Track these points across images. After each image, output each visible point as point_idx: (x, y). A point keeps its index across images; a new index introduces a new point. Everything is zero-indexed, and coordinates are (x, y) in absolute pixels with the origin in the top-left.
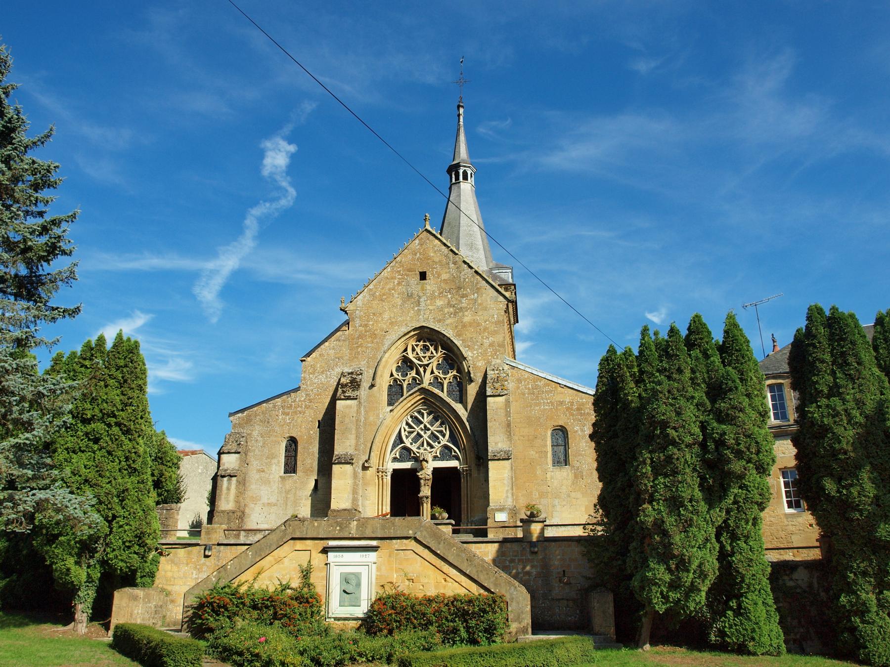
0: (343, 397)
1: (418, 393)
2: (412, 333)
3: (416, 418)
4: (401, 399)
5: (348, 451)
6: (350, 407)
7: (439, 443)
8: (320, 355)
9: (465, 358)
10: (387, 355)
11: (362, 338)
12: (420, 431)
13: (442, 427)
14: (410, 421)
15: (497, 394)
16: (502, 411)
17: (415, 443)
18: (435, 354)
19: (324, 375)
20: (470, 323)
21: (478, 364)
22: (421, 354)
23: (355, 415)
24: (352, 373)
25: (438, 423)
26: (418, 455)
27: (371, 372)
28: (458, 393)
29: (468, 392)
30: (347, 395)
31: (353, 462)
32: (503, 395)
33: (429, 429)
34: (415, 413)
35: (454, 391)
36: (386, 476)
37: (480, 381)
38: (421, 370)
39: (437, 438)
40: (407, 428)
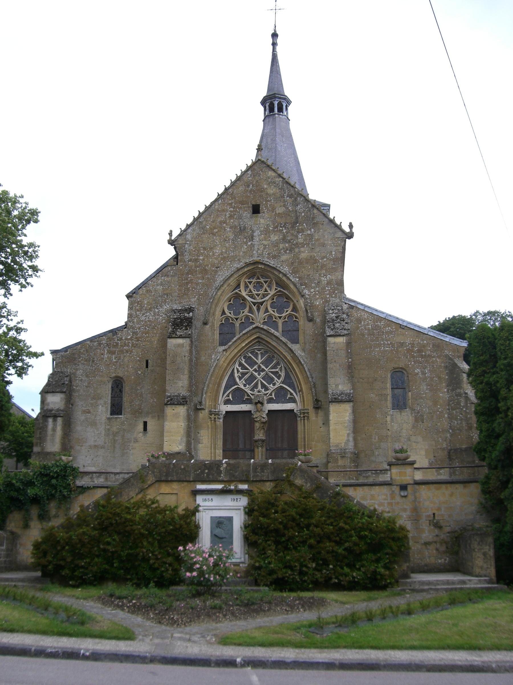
11: (192, 274)
20: (307, 259)
39: (273, 379)
40: (240, 368)
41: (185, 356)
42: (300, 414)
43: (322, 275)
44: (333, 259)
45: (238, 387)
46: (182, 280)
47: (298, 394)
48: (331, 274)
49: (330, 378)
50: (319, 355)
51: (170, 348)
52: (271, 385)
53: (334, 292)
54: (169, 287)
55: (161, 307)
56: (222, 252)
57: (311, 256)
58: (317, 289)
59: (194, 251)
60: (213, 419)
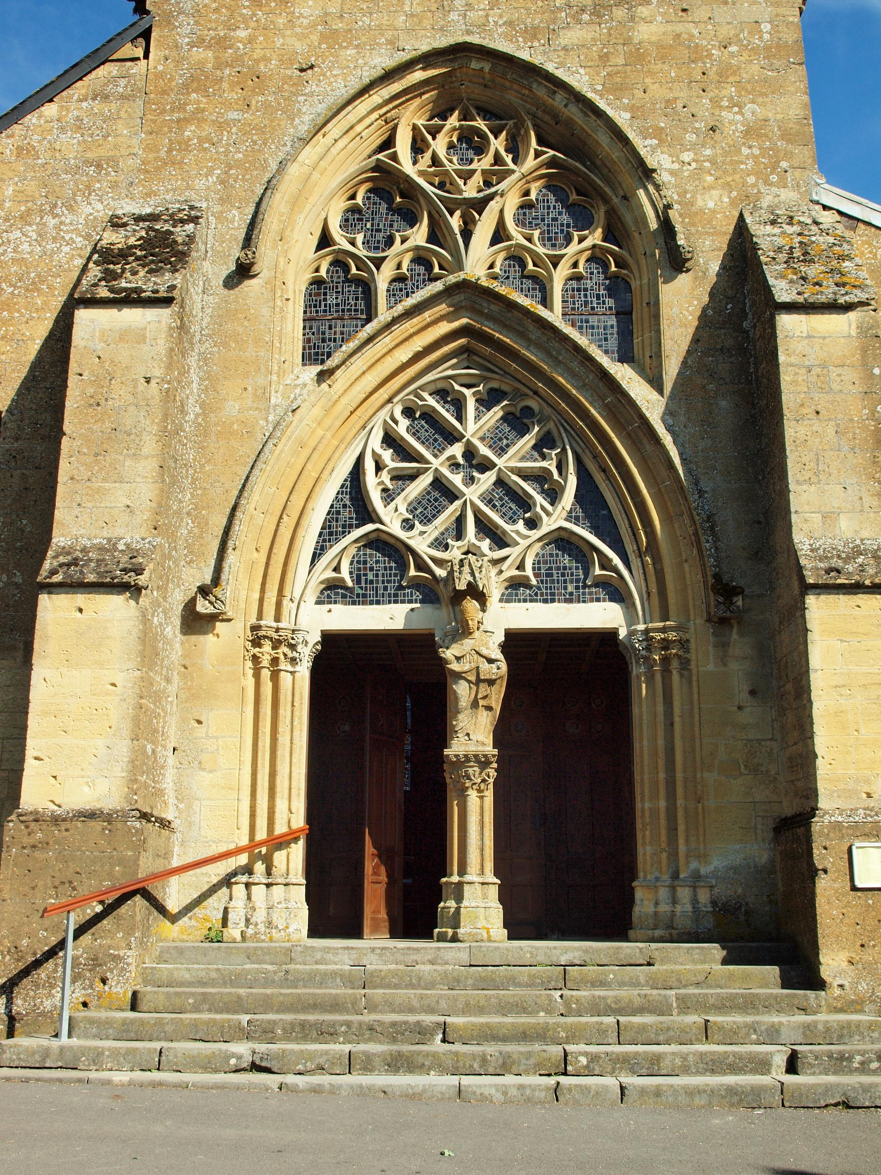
0: (103, 292)
1: (442, 308)
2: (419, 75)
3: (430, 417)
4: (370, 328)
5: (118, 532)
6: (140, 336)
7: (532, 524)
8: (20, 149)
9: (646, 173)
10: (309, 154)
11: (203, 90)
12: (445, 471)
13: (544, 457)
14: (402, 427)
15: (823, 299)
16: (851, 375)
17: (427, 520)
18: (512, 166)
19: (32, 231)
20: (660, 46)
21: (700, 203)
22: (452, 165)
23: (157, 372)
24: (153, 217)
25: (528, 440)
26: (440, 572)
27: (239, 220)
28: (613, 321)
29: (664, 311)
30: (124, 284)
31: (142, 580)
32: (848, 308)
33: (485, 466)
34: (425, 395)
35: (593, 312)
36: (293, 661)
37: (715, 267)
38: (455, 222)
39: (524, 503)
40: (387, 455)
41: (148, 380)
42: (648, 649)
43: (725, 103)
44: (767, 48)
45: (377, 530)
46: (164, 111)
47: (635, 562)
48: (760, 100)
49: (798, 483)
50: (724, 404)
51: (83, 343)
52: (520, 526)
53: (774, 167)
54: (105, 137)
55: (70, 209)
56: (326, 14)
57: (678, 36)
58: (708, 152)
59: (216, 10)
60: (265, 663)
